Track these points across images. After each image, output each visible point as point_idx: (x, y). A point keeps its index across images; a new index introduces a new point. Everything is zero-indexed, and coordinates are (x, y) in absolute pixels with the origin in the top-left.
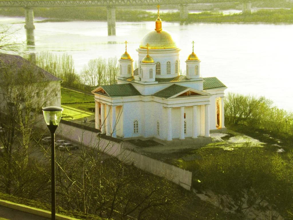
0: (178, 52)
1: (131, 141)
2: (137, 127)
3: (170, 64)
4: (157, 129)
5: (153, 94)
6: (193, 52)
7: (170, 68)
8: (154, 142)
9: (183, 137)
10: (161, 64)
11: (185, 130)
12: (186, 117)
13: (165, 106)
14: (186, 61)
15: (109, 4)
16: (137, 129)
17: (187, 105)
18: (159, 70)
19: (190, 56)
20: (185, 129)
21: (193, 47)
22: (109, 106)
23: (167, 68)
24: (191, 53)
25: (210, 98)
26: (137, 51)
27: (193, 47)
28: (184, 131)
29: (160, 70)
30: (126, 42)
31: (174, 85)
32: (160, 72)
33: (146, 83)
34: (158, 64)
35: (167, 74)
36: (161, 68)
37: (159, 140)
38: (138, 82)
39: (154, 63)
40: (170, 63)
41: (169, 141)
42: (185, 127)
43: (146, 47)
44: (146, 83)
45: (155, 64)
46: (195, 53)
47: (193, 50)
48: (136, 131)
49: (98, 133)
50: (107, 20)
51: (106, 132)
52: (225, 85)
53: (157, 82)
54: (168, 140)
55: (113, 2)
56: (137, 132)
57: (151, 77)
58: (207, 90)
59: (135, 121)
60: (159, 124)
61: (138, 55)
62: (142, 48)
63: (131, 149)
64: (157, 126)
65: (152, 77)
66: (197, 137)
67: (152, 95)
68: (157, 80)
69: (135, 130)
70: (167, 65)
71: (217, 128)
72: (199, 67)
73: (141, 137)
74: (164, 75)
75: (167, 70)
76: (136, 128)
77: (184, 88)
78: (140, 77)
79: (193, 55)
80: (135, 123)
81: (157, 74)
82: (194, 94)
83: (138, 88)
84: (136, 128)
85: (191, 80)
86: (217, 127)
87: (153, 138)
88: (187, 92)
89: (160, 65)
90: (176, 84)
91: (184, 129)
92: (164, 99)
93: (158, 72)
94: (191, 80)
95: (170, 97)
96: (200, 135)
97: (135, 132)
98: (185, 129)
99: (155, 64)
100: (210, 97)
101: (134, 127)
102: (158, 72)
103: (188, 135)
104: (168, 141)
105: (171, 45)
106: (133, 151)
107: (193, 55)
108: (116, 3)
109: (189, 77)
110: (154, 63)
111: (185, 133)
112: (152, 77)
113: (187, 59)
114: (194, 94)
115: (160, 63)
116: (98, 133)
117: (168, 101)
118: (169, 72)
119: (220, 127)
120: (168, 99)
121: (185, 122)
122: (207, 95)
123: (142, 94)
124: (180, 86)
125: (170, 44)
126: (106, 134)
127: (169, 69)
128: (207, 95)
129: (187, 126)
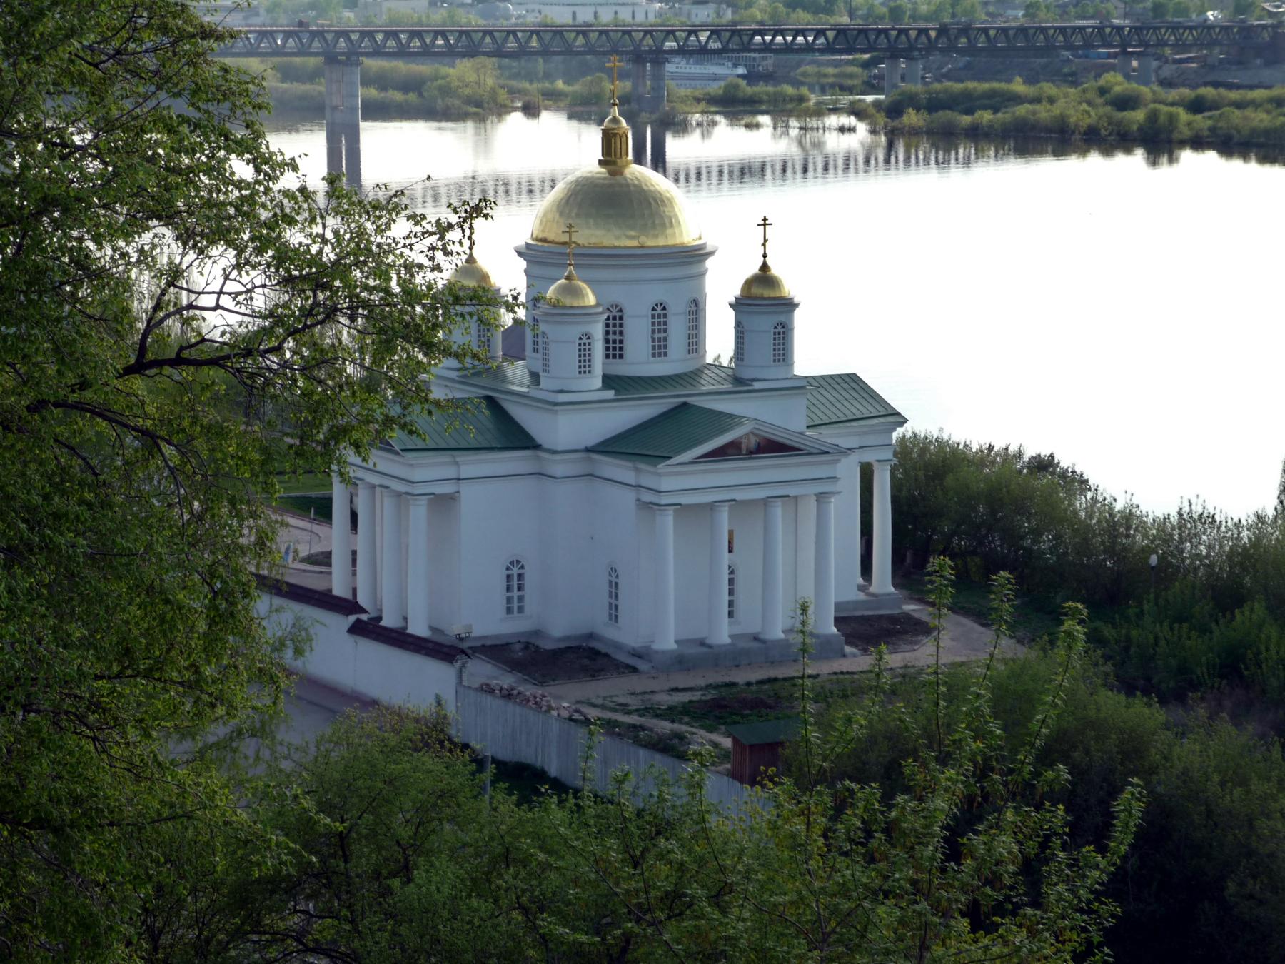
0: (704, 261)
1: (495, 651)
2: (520, 589)
3: (665, 316)
4: (610, 596)
5: (592, 440)
6: (765, 267)
7: (665, 331)
8: (594, 654)
9: (722, 634)
10: (627, 313)
11: (731, 604)
12: (735, 549)
13: (647, 497)
14: (733, 300)
15: (332, 46)
16: (521, 599)
17: (685, 500)
18: (618, 337)
19: (749, 284)
20: (731, 598)
21: (764, 245)
22: (399, 495)
23: (653, 331)
24: (754, 269)
25: (839, 465)
26: (520, 254)
27: (764, 245)
28: (726, 609)
29: (621, 342)
30: (765, 223)
31: (685, 404)
32: (621, 349)
33: (562, 398)
34: (615, 312)
35: (654, 355)
36: (627, 329)
37: (618, 646)
38: (524, 390)
39: (600, 310)
40: (664, 309)
41: (664, 652)
42: (731, 592)
43: (565, 238)
44: (562, 398)
45: (601, 313)
46: (775, 270)
47: (765, 256)
48: (515, 605)
49: (352, 618)
50: (324, 118)
51: (381, 610)
52: (899, 410)
53: (610, 394)
54: (657, 646)
55: (337, 41)
56: (521, 609)
57: (585, 367)
58: (824, 430)
59: (512, 563)
60: (617, 577)
61: (526, 271)
62: (537, 240)
63: (501, 690)
64: (610, 585)
65: (587, 369)
66: (674, 646)
67: (588, 450)
68: (609, 381)
69: (509, 600)
70: (653, 317)
71: (861, 596)
72: (792, 329)
73: (537, 633)
74: (638, 361)
75: (653, 340)
76: (515, 593)
77: (722, 421)
78: (534, 370)
79: (764, 278)
80: (509, 572)
81: (607, 356)
82: (772, 447)
83: (522, 415)
84: (515, 593)
85: (757, 385)
86: (861, 588)
87: (591, 636)
88: (743, 440)
89: (621, 318)
90: (690, 400)
91: (726, 598)
92: (642, 466)
93: (614, 349)
94: (757, 385)
95: (671, 458)
96: (706, 638)
97: (509, 610)
98: (731, 598)
99: (601, 313)
100: (838, 461)
101: (509, 589)
102: (614, 349)
103: (750, 622)
104: (657, 652)
105: (669, 231)
106: (508, 695)
107: (764, 278)
108: (362, 42)
109: (747, 374)
110: (600, 310)
111: (731, 614)
112: (587, 369)
113: (737, 291)
114: (772, 447)
115: (621, 311)
116: (352, 618)
117: (659, 475)
118: (660, 348)
119: (873, 589)
120: (660, 466)
121: (730, 567)
122: (827, 453)
123: (545, 446)
124: (698, 408)
125: (663, 226)
126: (380, 618)
127: (662, 335)
128: (827, 453)
129: (739, 586)
